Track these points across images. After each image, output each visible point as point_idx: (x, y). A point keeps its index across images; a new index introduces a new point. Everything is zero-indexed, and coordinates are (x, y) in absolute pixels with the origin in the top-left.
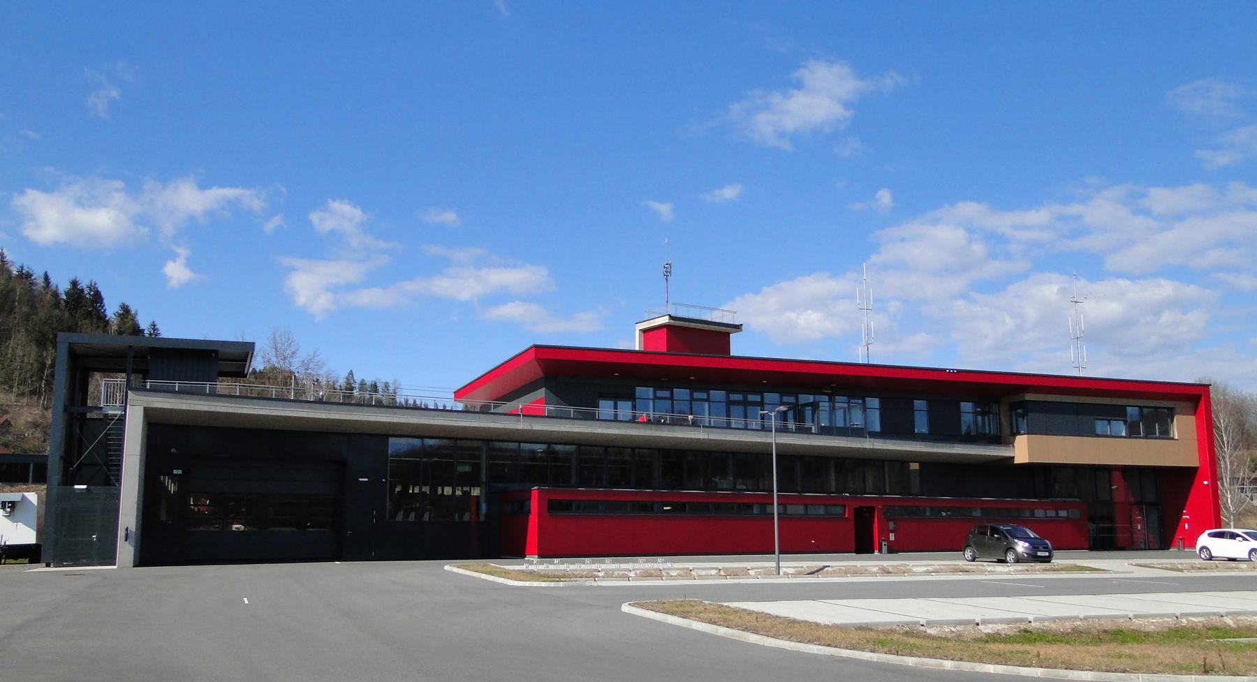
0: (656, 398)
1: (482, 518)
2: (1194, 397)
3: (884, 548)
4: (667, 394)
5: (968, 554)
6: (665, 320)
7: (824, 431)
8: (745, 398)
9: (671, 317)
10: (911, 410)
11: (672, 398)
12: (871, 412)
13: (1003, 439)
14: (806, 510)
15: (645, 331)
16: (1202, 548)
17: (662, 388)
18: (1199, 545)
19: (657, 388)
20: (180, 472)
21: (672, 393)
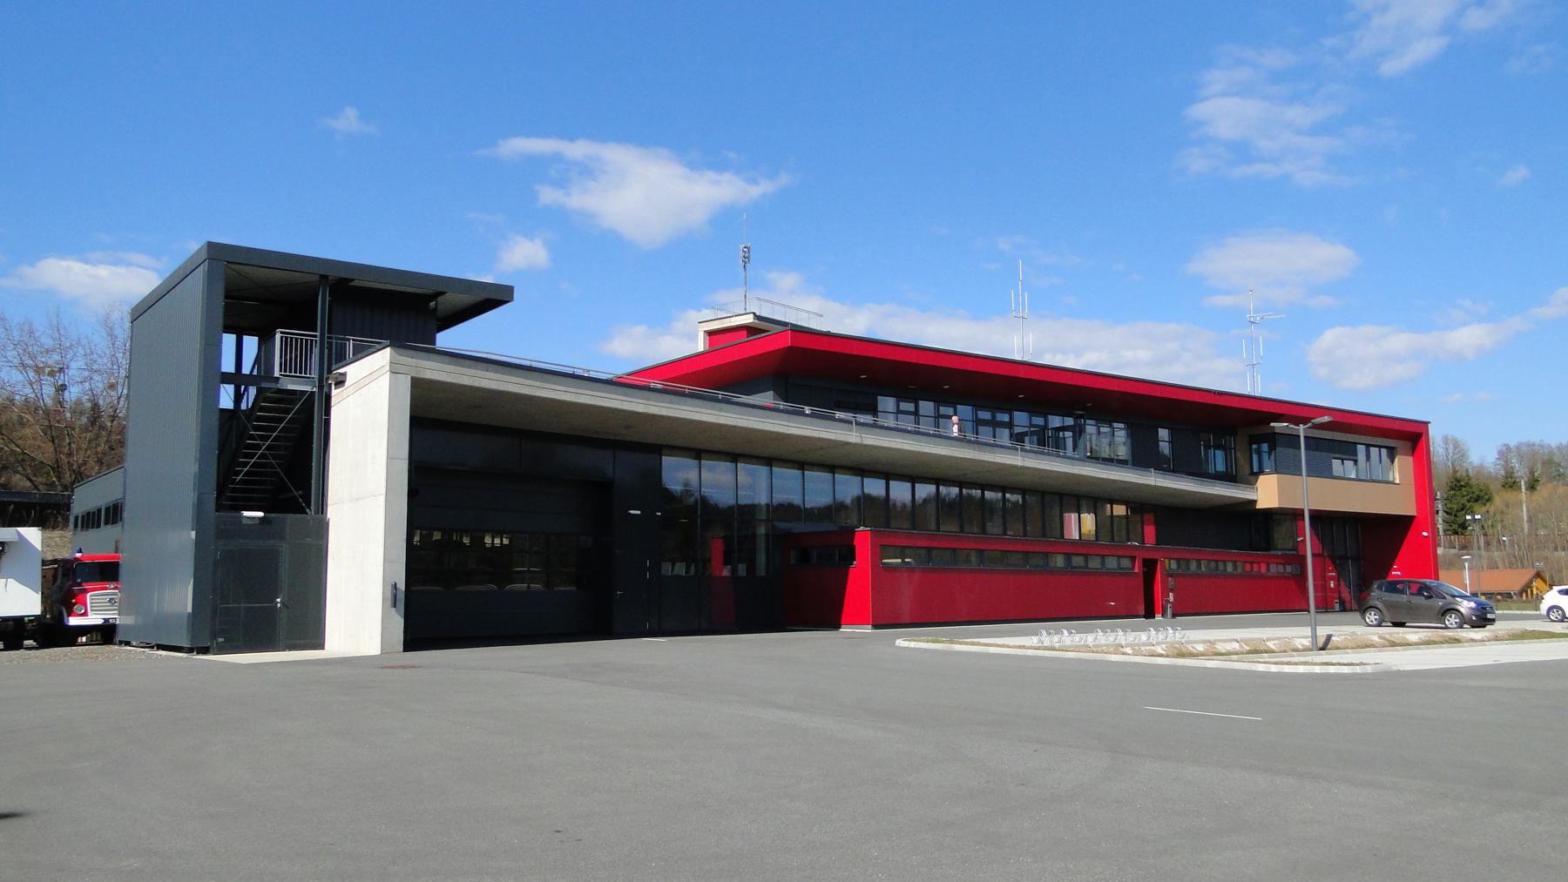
0: (899, 412)
1: (761, 571)
2: (1408, 437)
3: (1169, 611)
4: (910, 407)
5: (1372, 617)
6: (749, 319)
7: (1095, 458)
8: (994, 416)
9: (757, 317)
10: (1156, 440)
11: (916, 413)
12: (1118, 439)
13: (1250, 479)
14: (1103, 563)
15: (710, 333)
16: (1550, 609)
17: (907, 399)
18: (1544, 606)
19: (900, 397)
20: (1163, 433)
21: (917, 407)
